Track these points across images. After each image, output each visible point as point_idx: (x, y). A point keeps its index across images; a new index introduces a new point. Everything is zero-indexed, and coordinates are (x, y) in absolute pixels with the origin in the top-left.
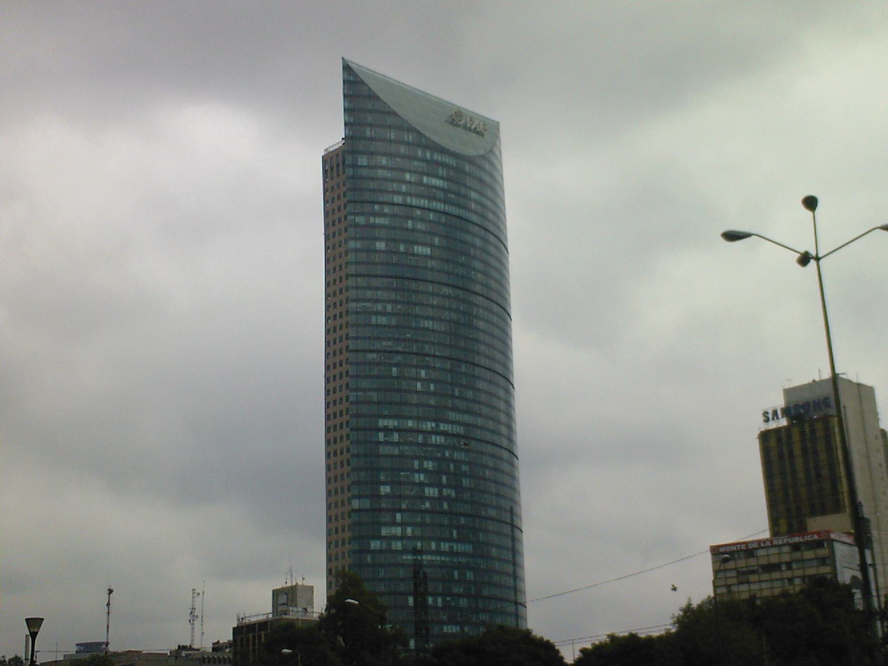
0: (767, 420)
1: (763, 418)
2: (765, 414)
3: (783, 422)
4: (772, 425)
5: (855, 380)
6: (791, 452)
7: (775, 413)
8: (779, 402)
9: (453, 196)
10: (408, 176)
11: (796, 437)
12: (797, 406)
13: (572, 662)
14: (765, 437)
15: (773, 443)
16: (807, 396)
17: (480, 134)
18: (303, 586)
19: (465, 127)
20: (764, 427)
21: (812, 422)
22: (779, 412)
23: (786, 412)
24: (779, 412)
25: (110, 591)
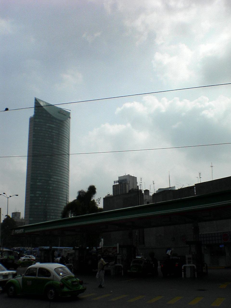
0: (114, 183)
1: (114, 182)
2: (114, 182)
3: (118, 184)
4: (115, 184)
5: (133, 176)
6: (118, 190)
7: (116, 181)
8: (117, 179)
9: (43, 181)
10: (40, 139)
11: (119, 187)
12: (120, 181)
13: (54, 253)
14: (114, 186)
15: (115, 188)
16: (123, 179)
17: (65, 115)
18: (18, 212)
19: (62, 114)
20: (114, 184)
21: (122, 184)
22: (117, 181)
23: (118, 181)
24: (117, 181)
25: (200, 174)
